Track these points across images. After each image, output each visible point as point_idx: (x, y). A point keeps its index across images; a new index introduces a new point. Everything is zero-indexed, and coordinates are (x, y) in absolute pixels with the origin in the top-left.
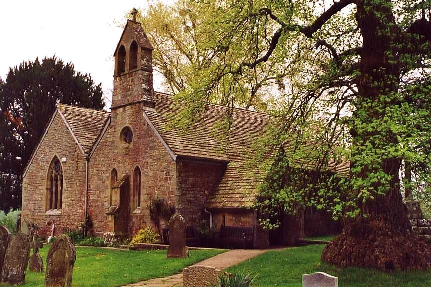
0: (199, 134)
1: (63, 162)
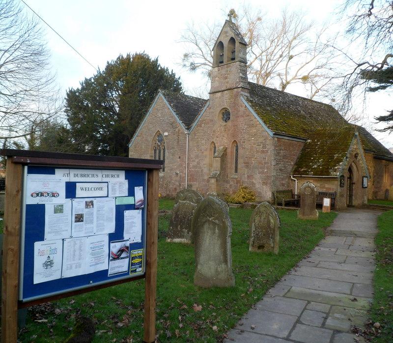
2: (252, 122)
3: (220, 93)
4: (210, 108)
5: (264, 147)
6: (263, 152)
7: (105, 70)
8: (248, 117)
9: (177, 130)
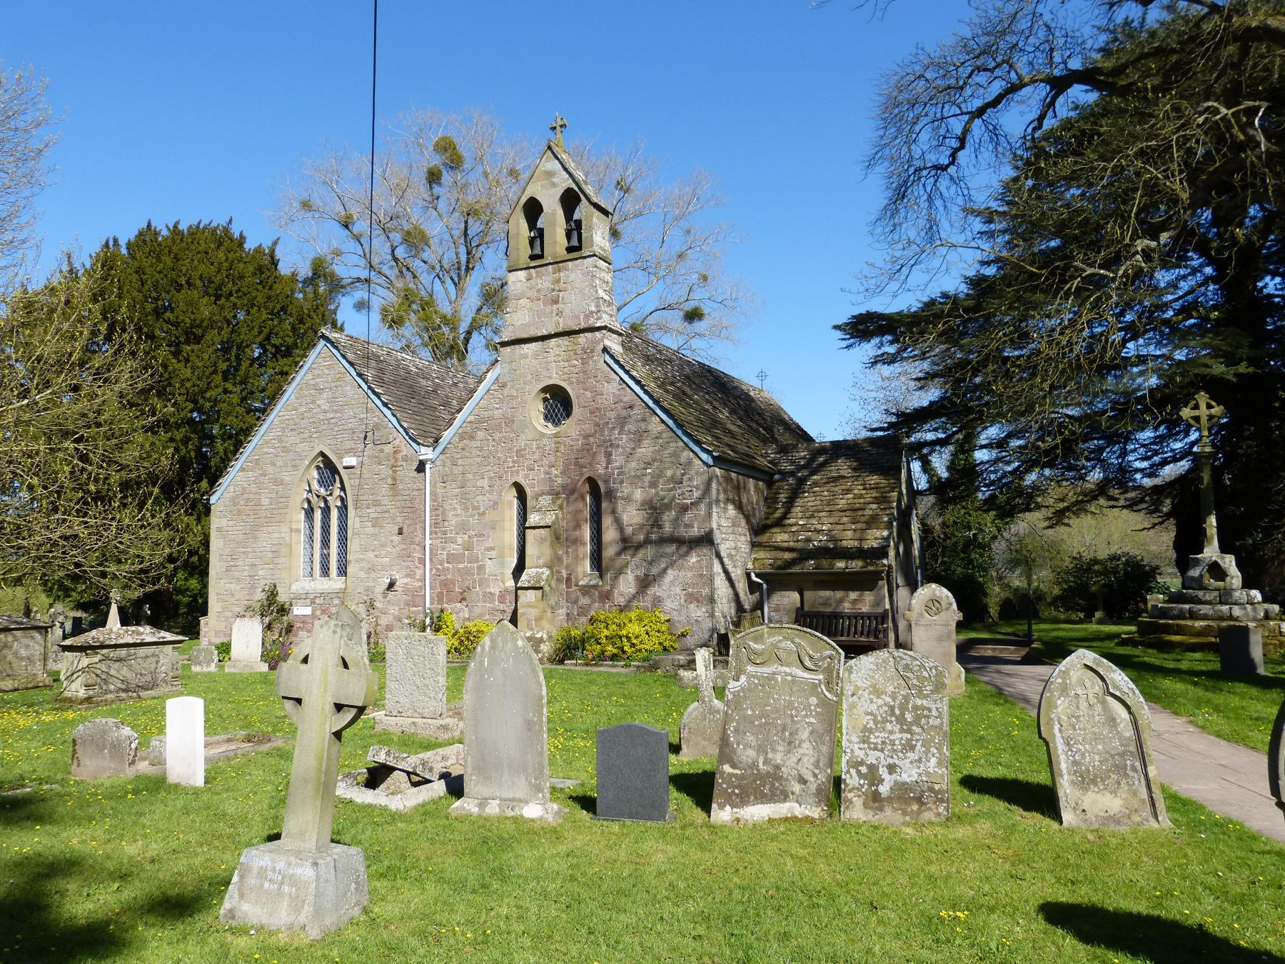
1: (345, 468)
4: (504, 386)
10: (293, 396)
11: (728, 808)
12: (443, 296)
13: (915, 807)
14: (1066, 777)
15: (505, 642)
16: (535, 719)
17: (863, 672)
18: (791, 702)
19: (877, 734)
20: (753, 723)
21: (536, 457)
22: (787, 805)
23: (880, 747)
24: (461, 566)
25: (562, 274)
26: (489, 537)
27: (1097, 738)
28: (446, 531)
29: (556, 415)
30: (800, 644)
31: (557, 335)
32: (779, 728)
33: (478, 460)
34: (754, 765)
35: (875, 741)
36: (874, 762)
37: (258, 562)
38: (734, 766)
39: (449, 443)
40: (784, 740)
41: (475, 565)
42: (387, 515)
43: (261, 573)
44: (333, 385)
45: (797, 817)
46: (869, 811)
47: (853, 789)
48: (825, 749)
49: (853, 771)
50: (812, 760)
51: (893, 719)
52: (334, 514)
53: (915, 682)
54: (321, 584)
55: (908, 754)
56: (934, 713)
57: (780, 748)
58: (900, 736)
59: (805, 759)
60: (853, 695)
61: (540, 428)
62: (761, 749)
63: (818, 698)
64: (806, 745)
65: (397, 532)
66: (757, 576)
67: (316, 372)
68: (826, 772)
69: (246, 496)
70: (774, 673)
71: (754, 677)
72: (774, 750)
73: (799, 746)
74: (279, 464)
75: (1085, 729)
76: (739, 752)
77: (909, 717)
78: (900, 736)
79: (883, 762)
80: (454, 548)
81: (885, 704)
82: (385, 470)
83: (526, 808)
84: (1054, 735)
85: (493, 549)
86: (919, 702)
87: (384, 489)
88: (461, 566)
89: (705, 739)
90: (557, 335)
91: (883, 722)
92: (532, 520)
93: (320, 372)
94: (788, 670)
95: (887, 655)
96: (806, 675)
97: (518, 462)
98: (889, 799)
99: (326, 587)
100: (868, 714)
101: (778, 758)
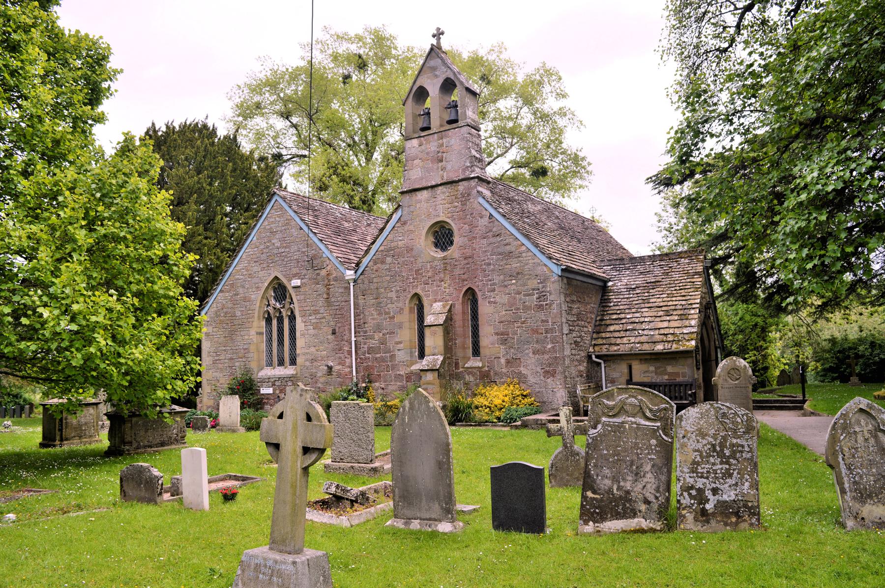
0: (647, 283)
1: (294, 287)
2: (508, 247)
3: (425, 192)
4: (405, 223)
5: (542, 296)
6: (540, 307)
7: (176, 125)
8: (499, 239)
9: (323, 273)
10: (255, 238)
11: (591, 523)
12: (356, 162)
13: (734, 520)
14: (848, 494)
15: (420, 404)
16: (444, 460)
17: (691, 420)
18: (636, 444)
19: (703, 466)
20: (608, 460)
21: (430, 274)
22: (636, 520)
23: (705, 475)
24: (378, 356)
25: (444, 140)
26: (397, 334)
27: (871, 463)
28: (366, 331)
29: (444, 243)
30: (641, 400)
31: (441, 185)
32: (628, 463)
33: (388, 278)
34: (610, 491)
35: (702, 471)
36: (702, 486)
37: (234, 356)
38: (594, 492)
39: (366, 267)
40: (632, 472)
41: (388, 355)
42: (324, 320)
43: (237, 364)
44: (283, 228)
45: (643, 529)
46: (698, 523)
47: (686, 507)
48: (663, 478)
49: (685, 494)
50: (654, 486)
51: (715, 454)
52: (286, 322)
53: (731, 425)
54: (280, 371)
55: (727, 480)
56: (747, 449)
57: (630, 478)
58: (720, 467)
59: (649, 486)
60: (684, 437)
61: (432, 254)
62: (615, 479)
63: (657, 440)
64: (649, 475)
65: (331, 332)
66: (597, 357)
67: (271, 220)
68: (665, 495)
69: (225, 310)
70: (623, 423)
71: (607, 425)
72: (624, 480)
73: (644, 476)
74: (247, 286)
75: (862, 457)
76: (598, 482)
77: (727, 452)
78: (720, 467)
79: (708, 486)
80: (373, 343)
81: (708, 443)
82: (321, 288)
83: (439, 525)
84: (839, 463)
85: (400, 343)
86: (735, 441)
87: (321, 302)
88: (378, 356)
89: (568, 475)
90: (441, 185)
91: (707, 457)
92: (429, 321)
93: (273, 220)
94: (633, 420)
95: (709, 406)
96: (647, 423)
97: (417, 278)
98: (713, 514)
99: (282, 373)
100: (696, 451)
101: (628, 486)
